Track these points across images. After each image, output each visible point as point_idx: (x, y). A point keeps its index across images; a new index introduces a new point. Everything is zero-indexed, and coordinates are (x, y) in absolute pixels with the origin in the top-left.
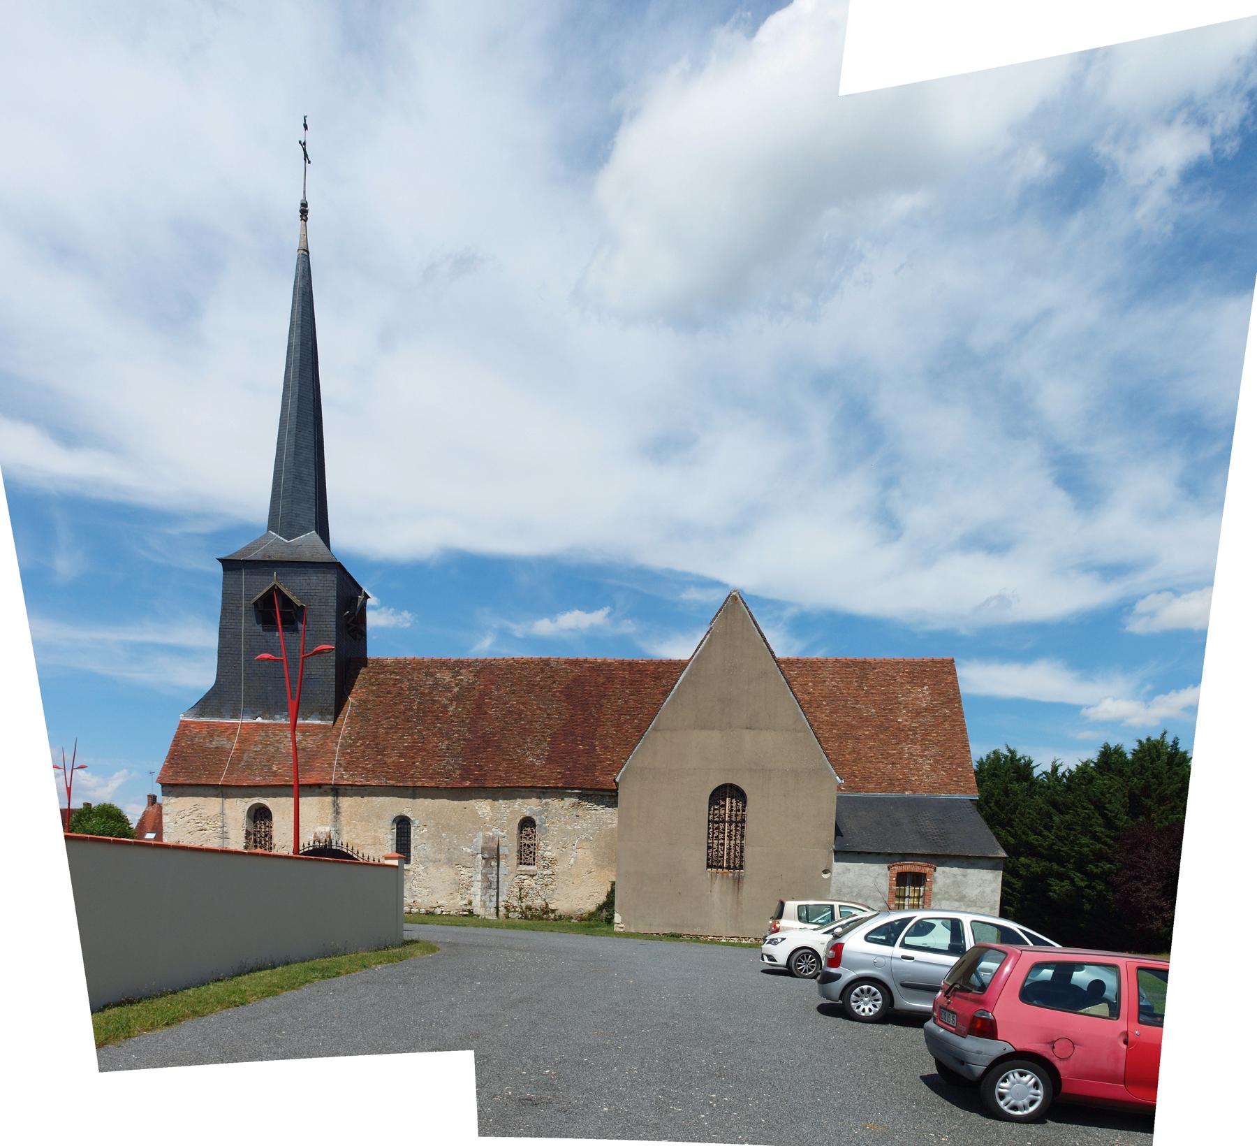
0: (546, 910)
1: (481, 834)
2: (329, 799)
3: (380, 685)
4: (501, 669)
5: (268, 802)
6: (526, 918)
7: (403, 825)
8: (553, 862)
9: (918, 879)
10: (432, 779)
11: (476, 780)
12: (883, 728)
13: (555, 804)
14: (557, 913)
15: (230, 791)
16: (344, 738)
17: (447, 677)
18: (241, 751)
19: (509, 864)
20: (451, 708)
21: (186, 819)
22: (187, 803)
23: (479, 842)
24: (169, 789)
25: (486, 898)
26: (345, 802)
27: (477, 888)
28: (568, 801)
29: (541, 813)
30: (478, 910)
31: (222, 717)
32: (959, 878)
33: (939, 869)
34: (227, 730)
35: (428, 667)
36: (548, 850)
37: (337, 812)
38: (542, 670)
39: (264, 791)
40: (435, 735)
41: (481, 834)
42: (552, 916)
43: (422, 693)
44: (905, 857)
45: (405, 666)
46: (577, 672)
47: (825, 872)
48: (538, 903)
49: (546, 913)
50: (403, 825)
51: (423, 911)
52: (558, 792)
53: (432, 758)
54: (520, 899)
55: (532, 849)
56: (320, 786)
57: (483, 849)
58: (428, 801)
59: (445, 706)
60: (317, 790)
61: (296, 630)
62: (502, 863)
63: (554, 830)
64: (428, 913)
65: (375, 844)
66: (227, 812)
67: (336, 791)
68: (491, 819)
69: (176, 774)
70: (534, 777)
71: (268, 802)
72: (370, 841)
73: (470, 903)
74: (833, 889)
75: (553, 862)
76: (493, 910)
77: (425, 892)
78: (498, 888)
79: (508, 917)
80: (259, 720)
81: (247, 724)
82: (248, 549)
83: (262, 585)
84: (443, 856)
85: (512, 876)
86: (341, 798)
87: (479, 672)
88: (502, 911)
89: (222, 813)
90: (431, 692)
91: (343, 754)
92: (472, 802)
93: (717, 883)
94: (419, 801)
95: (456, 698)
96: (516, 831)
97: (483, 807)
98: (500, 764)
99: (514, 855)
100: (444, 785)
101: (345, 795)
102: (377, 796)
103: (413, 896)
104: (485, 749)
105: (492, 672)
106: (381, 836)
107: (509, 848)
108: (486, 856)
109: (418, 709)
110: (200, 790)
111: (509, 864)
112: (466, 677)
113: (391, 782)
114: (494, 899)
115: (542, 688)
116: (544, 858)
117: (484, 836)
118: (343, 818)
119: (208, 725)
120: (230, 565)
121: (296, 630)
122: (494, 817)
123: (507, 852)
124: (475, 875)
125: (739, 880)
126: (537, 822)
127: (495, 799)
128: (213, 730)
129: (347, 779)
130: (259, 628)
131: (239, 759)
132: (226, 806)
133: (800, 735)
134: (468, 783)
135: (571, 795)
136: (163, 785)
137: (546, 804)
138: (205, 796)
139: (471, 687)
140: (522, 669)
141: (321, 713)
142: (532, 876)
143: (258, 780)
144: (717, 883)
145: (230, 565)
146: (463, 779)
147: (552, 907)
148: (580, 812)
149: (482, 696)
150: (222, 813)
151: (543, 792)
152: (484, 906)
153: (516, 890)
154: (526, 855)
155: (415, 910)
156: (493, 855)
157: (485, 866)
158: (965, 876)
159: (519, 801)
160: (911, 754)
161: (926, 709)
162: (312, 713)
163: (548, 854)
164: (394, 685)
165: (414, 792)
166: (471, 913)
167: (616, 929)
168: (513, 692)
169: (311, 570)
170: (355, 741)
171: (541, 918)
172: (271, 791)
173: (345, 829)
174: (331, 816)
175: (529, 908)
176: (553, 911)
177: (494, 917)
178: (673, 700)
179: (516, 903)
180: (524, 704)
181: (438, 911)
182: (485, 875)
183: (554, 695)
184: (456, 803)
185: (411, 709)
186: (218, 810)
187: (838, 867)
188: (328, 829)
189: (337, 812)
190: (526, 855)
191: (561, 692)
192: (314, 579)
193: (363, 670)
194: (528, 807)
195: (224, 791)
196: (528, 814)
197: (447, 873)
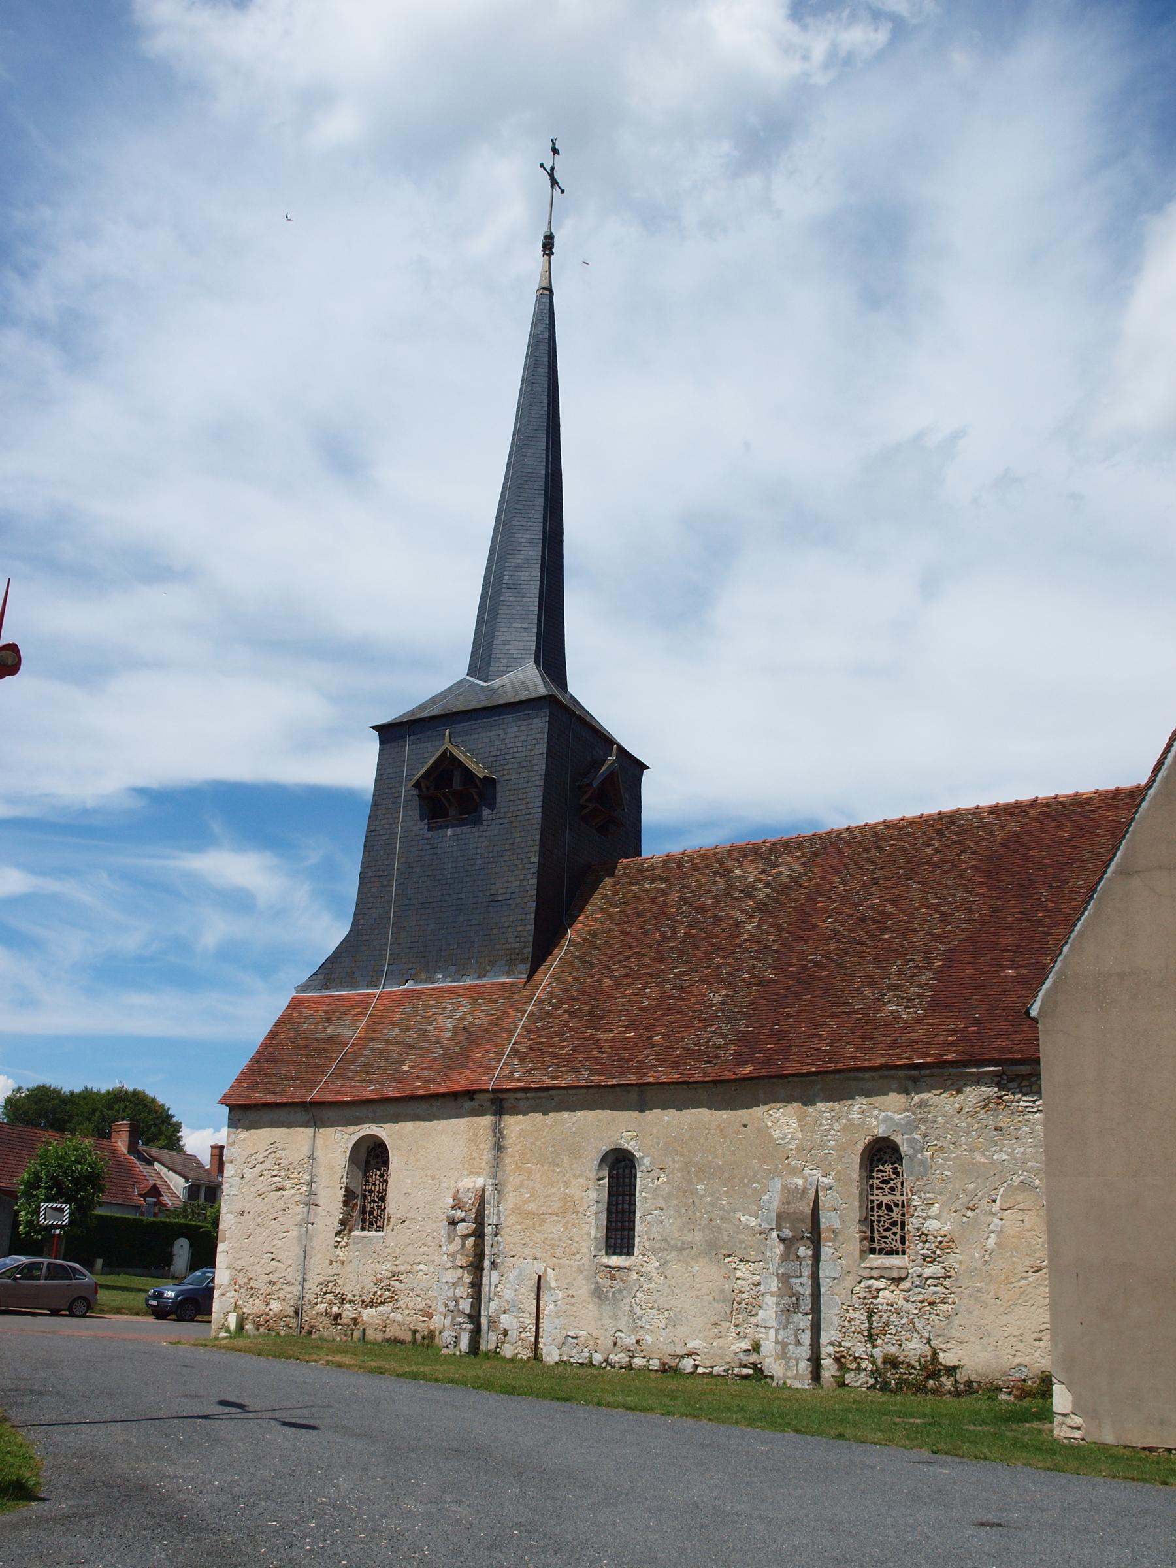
0: (933, 1368)
1: (777, 1184)
2: (487, 1120)
3: (629, 902)
4: (857, 845)
5: (383, 1132)
6: (885, 1387)
7: (620, 1168)
8: (946, 1244)
10: (676, 1066)
11: (768, 1061)
13: (943, 1104)
14: (961, 1376)
15: (331, 1114)
16: (539, 1003)
17: (751, 873)
18: (365, 1040)
19: (842, 1253)
20: (748, 927)
21: (259, 1168)
22: (261, 1138)
23: (773, 1199)
24: (238, 1115)
25: (787, 1335)
26: (514, 1125)
27: (768, 1312)
28: (973, 1095)
29: (912, 1126)
30: (773, 1366)
31: (354, 986)
34: (354, 1007)
35: (721, 861)
36: (933, 1218)
37: (499, 1147)
38: (941, 833)
39: (380, 1110)
40: (704, 980)
41: (777, 1184)
42: (947, 1382)
43: (702, 908)
45: (680, 865)
46: (1014, 826)
48: (914, 1349)
49: (935, 1375)
50: (620, 1168)
51: (655, 1364)
52: (946, 1073)
53: (689, 1024)
54: (871, 1338)
55: (896, 1214)
56: (470, 1094)
57: (779, 1216)
58: (669, 1116)
59: (738, 925)
60: (468, 1105)
61: (478, 821)
62: (826, 1250)
63: (944, 1166)
64: (667, 1370)
65: (563, 1212)
66: (319, 1153)
67: (499, 1103)
68: (800, 1148)
69: (252, 1088)
70: (894, 1044)
71: (383, 1132)
72: (556, 1206)
73: (756, 1348)
75: (946, 1244)
76: (804, 1366)
77: (661, 1320)
78: (816, 1310)
79: (842, 1384)
81: (389, 994)
83: (427, 754)
84: (698, 1237)
85: (849, 1282)
86: (506, 1117)
87: (815, 855)
88: (829, 1367)
89: (311, 1157)
90: (716, 904)
91: (528, 1030)
92: (759, 1111)
94: (652, 1115)
95: (763, 908)
96: (855, 1172)
97: (782, 1121)
98: (822, 1025)
99: (853, 1232)
100: (698, 1077)
101: (515, 1111)
102: (572, 1108)
103: (636, 1329)
104: (798, 997)
105: (839, 853)
106: (577, 1193)
107: (842, 1215)
108: (787, 1233)
109: (687, 935)
110: (282, 1114)
111: (842, 1253)
112: (788, 867)
113: (597, 1079)
114: (806, 1338)
115: (935, 867)
116: (923, 1236)
117: (785, 1187)
118: (510, 1160)
119: (330, 1001)
120: (389, 733)
121: (478, 821)
122: (806, 1142)
123: (837, 1224)
124: (762, 1277)
126: (904, 1149)
127: (808, 1101)
128: (335, 1010)
129: (520, 1077)
130: (424, 825)
131: (356, 1054)
132: (320, 1142)
134: (747, 1070)
135: (978, 1080)
136: (232, 1108)
137: (923, 1104)
138: (289, 1125)
139: (795, 883)
140: (899, 837)
141: (510, 962)
142: (898, 1281)
143: (372, 1090)
145: (389, 733)
146: (740, 1059)
147: (947, 1359)
148: (1005, 1120)
149: (812, 898)
150: (311, 1157)
151: (913, 1076)
152: (783, 1355)
153: (860, 1316)
154: (883, 1229)
155: (639, 1362)
156: (806, 1230)
157: (785, 1258)
159: (861, 1102)
162: (493, 963)
163: (932, 1225)
164: (654, 899)
165: (642, 1097)
166: (758, 1370)
167: (1061, 1432)
168: (875, 882)
169: (508, 718)
170: (556, 1007)
171: (920, 1389)
172: (391, 1109)
173: (512, 1181)
174: (488, 1156)
175: (892, 1362)
176: (951, 1370)
177: (806, 1384)
179: (860, 1349)
180: (895, 901)
181: (687, 1364)
182: (784, 1279)
183: (960, 876)
184: (726, 1115)
185: (673, 937)
186: (305, 1151)
188: (480, 1182)
189: (499, 1147)
190: (883, 1229)
191: (976, 869)
192: (512, 731)
193: (607, 881)
194: (883, 1113)
195: (316, 1113)
196: (881, 1131)
197: (705, 1275)
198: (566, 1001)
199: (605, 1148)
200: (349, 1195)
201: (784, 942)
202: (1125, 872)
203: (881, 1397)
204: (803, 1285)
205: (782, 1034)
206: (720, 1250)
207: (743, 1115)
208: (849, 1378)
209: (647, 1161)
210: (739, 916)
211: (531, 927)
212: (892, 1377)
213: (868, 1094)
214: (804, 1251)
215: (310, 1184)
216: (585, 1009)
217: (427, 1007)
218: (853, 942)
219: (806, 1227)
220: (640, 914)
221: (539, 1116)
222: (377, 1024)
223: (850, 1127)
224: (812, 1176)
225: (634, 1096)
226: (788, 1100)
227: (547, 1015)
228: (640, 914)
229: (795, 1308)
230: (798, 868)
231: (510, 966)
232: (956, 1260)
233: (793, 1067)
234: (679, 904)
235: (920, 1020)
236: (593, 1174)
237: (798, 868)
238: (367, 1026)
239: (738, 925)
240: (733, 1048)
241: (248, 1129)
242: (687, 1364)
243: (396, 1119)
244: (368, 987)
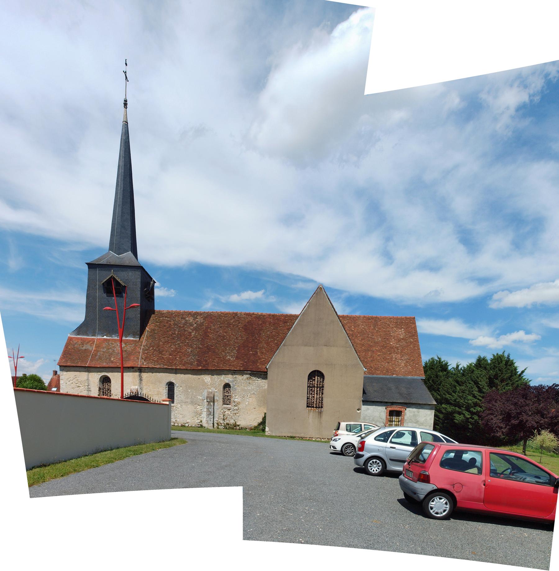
0: (235, 425)
1: (206, 391)
2: (137, 374)
3: (161, 322)
4: (215, 317)
5: (109, 375)
6: (226, 428)
7: (171, 386)
8: (239, 403)
9: (399, 414)
10: (184, 365)
11: (204, 366)
12: (384, 347)
13: (239, 377)
14: (240, 426)
17: (191, 320)
18: (97, 351)
19: (219, 404)
21: (71, 382)
23: (205, 394)
24: (63, 368)
25: (208, 419)
26: (145, 375)
27: (204, 414)
28: (245, 376)
29: (233, 381)
30: (205, 424)
31: (88, 335)
32: (416, 413)
33: (407, 409)
35: (183, 315)
36: (236, 398)
37: (141, 380)
38: (234, 317)
39: (107, 370)
41: (206, 391)
42: (238, 428)
44: (393, 403)
45: (172, 314)
46: (249, 319)
47: (358, 410)
48: (232, 422)
50: (171, 386)
51: (180, 425)
52: (241, 372)
53: (184, 356)
55: (229, 397)
56: (133, 368)
57: (207, 397)
58: (182, 376)
59: (190, 333)
60: (132, 370)
62: (216, 404)
65: (158, 394)
66: (90, 379)
67: (140, 370)
68: (211, 384)
69: (66, 361)
70: (230, 365)
71: (109, 375)
73: (201, 422)
74: (361, 418)
75: (239, 403)
76: (212, 425)
77: (181, 416)
78: (214, 415)
79: (218, 428)
80: (105, 337)
82: (100, 259)
83: (106, 276)
84: (189, 400)
85: (220, 409)
87: (206, 317)
88: (216, 425)
89: (88, 379)
90: (184, 326)
91: (144, 353)
92: (202, 376)
93: (311, 414)
94: (178, 375)
95: (195, 329)
96: (222, 389)
97: (207, 378)
98: (214, 359)
100: (189, 368)
101: (144, 372)
102: (159, 372)
103: (175, 418)
105: (211, 318)
107: (219, 397)
108: (209, 400)
109: (178, 334)
111: (219, 404)
112: (200, 320)
113: (166, 367)
114: (212, 420)
115: (234, 326)
116: (234, 402)
117: (208, 391)
118: (144, 382)
121: (122, 297)
122: (212, 383)
124: (204, 409)
125: (321, 413)
126: (231, 385)
127: (213, 375)
128: (83, 341)
129: (145, 365)
130: (105, 295)
131: (96, 355)
133: (348, 349)
134: (200, 368)
135: (246, 374)
136: (60, 366)
137: (235, 377)
139: (202, 324)
141: (134, 335)
142: (229, 410)
143: (105, 364)
144: (311, 414)
145: (91, 266)
146: (198, 365)
147: (238, 423)
148: (251, 381)
150: (88, 379)
151: (234, 372)
152: (207, 423)
154: (227, 400)
155: (176, 424)
156: (212, 400)
157: (208, 405)
158: (418, 412)
159: (223, 376)
160: (396, 358)
161: (403, 339)
163: (236, 400)
164: (167, 322)
165: (176, 371)
167: (266, 434)
169: (129, 270)
170: (149, 348)
171: (233, 429)
174: (138, 381)
175: (228, 424)
176: (238, 425)
177: (212, 428)
178: (292, 332)
179: (222, 422)
180: (225, 332)
181: (187, 425)
182: (208, 409)
183: (239, 329)
184: (195, 376)
185: (175, 334)
186: (86, 378)
187: (364, 408)
188: (137, 387)
189: (141, 380)
190: (227, 400)
191: (242, 328)
193: (153, 316)
194: (228, 378)
197: (191, 407)
198: (151, 346)
199: (167, 381)
200: (100, 389)
201: (202, 339)
202: (284, 345)
203: (226, 430)
204: (211, 410)
205: (206, 361)
206: (193, 403)
207: (199, 377)
208: (219, 427)
209: (177, 385)
210: (191, 331)
211: (139, 327)
212: (227, 426)
213: (225, 375)
214: (212, 404)
215: (88, 386)
216: (157, 349)
217: (112, 344)
218: (218, 341)
219: (212, 399)
220: (165, 326)
221: (151, 374)
222: (99, 347)
223: (221, 380)
224: (213, 390)
225: (174, 371)
226: (209, 374)
227: (147, 350)
228: (165, 326)
229: (210, 414)
230: (202, 321)
231: (134, 335)
232: (240, 406)
233: (210, 368)
234: (174, 324)
235: (235, 361)
236: (165, 387)
237: (202, 321)
238: (96, 347)
239: (190, 333)
240: (196, 363)
241: (67, 372)
242: (187, 425)
243: (112, 372)
244: (92, 336)
